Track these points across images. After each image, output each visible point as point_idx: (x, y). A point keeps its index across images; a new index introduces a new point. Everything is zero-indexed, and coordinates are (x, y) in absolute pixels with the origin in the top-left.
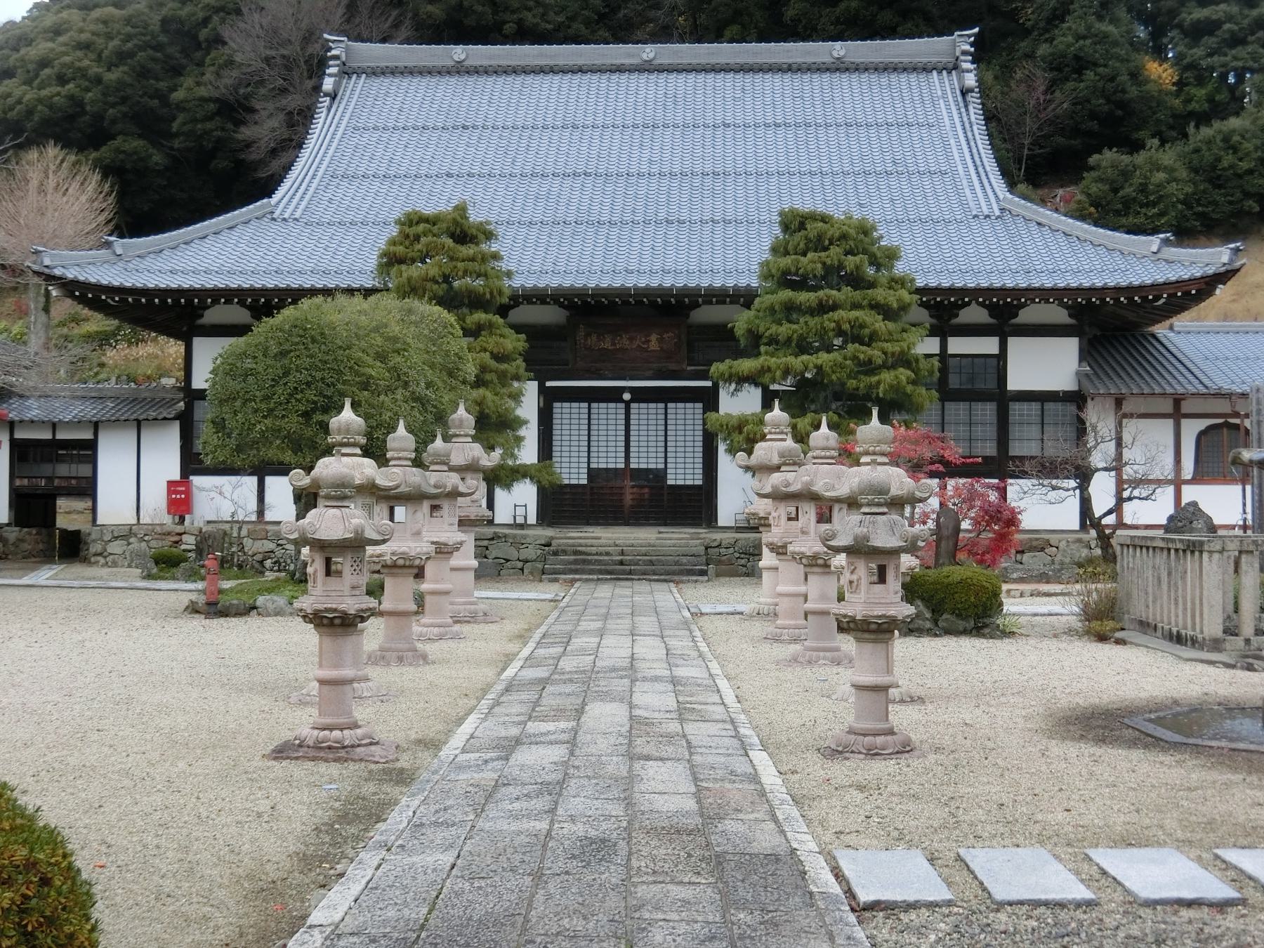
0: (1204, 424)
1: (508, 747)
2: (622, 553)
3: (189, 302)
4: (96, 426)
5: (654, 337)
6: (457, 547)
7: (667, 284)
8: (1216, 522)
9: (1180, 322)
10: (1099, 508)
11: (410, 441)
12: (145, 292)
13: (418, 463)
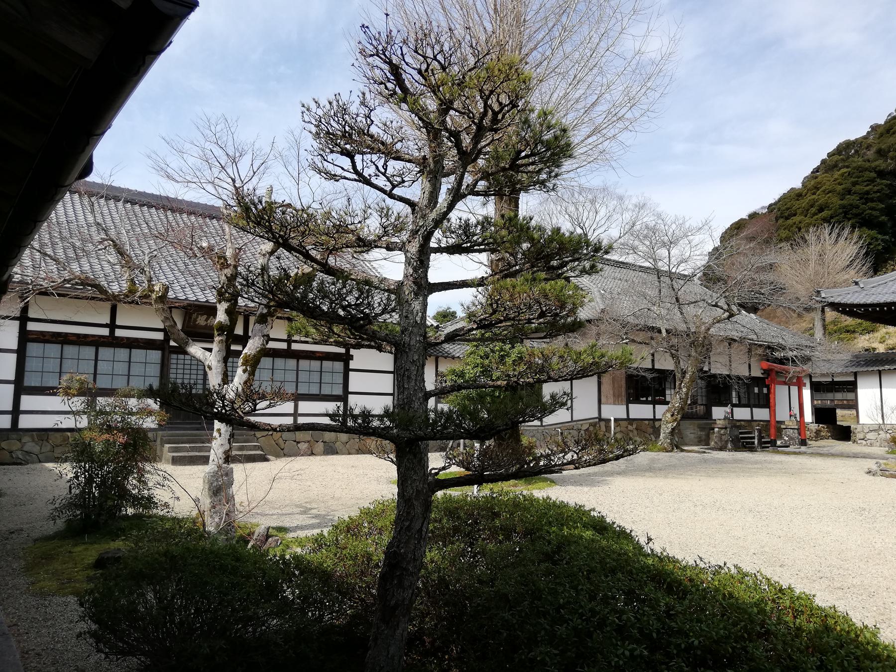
4: (855, 374)
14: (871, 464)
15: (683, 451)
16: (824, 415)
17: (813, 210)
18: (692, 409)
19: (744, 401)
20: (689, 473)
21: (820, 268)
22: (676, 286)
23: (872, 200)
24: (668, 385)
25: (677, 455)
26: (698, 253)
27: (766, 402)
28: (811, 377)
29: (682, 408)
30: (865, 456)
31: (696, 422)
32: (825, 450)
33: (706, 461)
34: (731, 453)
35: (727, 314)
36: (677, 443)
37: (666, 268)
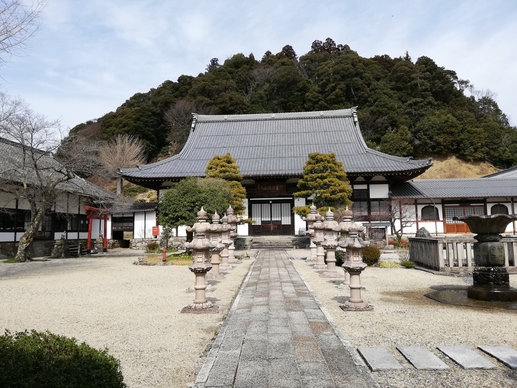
0: (423, 206)
1: (250, 307)
2: (271, 243)
3: (158, 181)
4: (134, 213)
5: (277, 187)
6: (230, 244)
7: (280, 173)
8: (430, 232)
9: (415, 180)
10: (397, 230)
11: (218, 217)
12: (147, 178)
13: (220, 223)
14: (136, 259)
15: (32, 260)
16: (117, 235)
17: (121, 125)
18: (41, 234)
19: (74, 229)
20: (34, 274)
21: (122, 157)
22: (35, 157)
23: (149, 126)
24: (26, 219)
25: (28, 264)
26: (51, 139)
27: (86, 229)
28: (112, 215)
29: (34, 234)
30: (135, 255)
31: (44, 242)
32: (116, 254)
33: (46, 266)
34: (63, 259)
35: (67, 177)
36: (29, 255)
37: (29, 145)
